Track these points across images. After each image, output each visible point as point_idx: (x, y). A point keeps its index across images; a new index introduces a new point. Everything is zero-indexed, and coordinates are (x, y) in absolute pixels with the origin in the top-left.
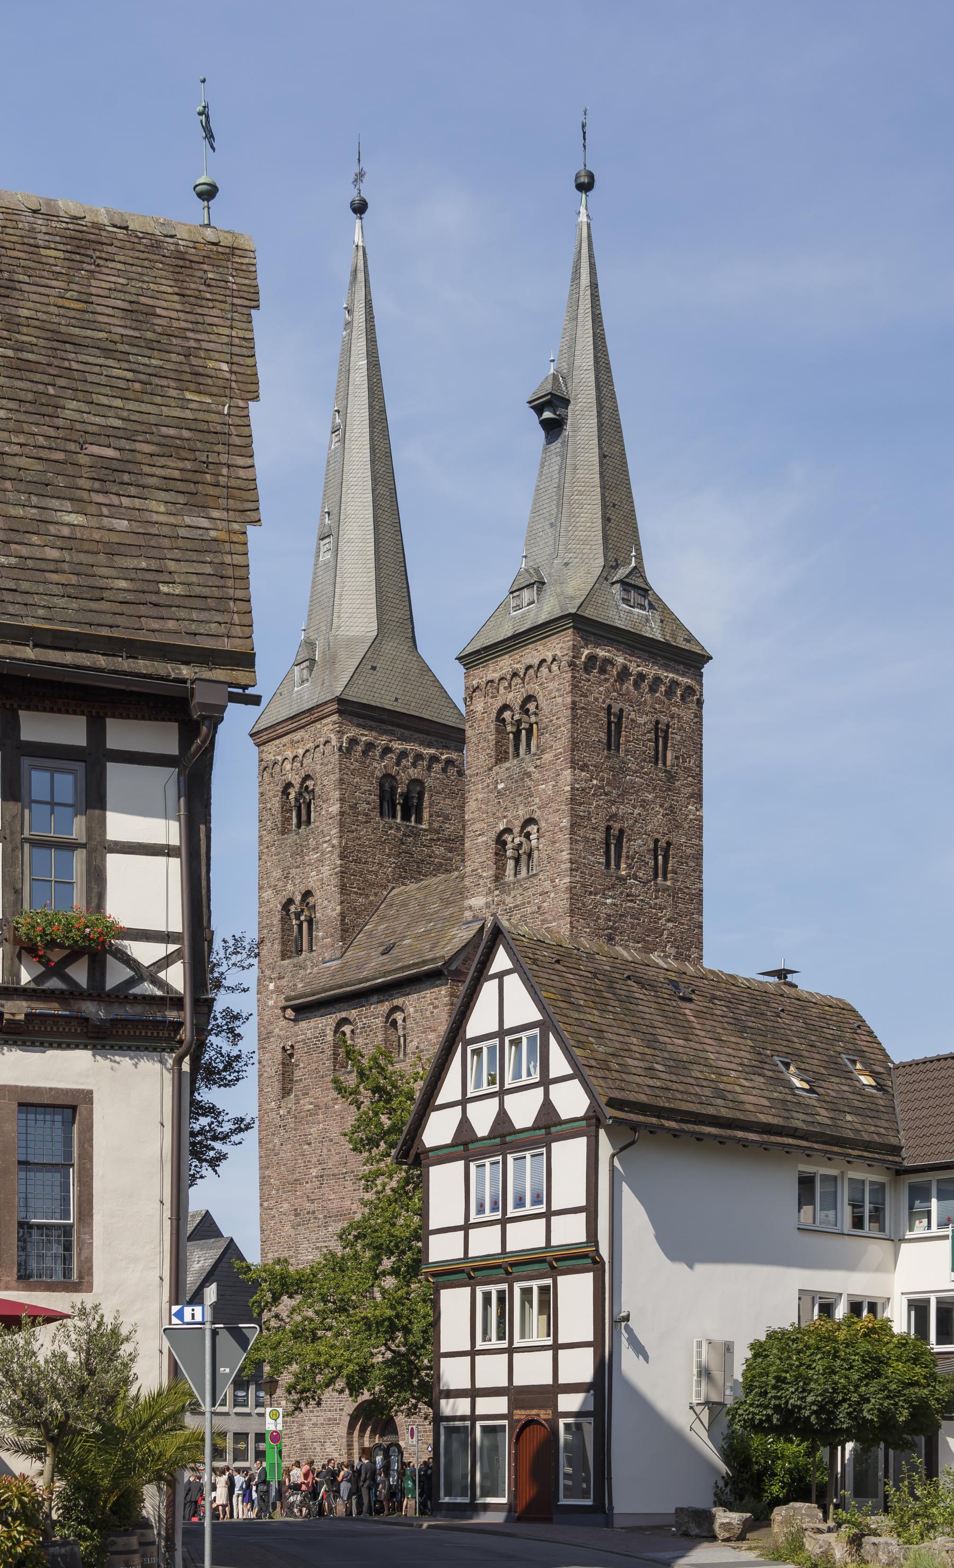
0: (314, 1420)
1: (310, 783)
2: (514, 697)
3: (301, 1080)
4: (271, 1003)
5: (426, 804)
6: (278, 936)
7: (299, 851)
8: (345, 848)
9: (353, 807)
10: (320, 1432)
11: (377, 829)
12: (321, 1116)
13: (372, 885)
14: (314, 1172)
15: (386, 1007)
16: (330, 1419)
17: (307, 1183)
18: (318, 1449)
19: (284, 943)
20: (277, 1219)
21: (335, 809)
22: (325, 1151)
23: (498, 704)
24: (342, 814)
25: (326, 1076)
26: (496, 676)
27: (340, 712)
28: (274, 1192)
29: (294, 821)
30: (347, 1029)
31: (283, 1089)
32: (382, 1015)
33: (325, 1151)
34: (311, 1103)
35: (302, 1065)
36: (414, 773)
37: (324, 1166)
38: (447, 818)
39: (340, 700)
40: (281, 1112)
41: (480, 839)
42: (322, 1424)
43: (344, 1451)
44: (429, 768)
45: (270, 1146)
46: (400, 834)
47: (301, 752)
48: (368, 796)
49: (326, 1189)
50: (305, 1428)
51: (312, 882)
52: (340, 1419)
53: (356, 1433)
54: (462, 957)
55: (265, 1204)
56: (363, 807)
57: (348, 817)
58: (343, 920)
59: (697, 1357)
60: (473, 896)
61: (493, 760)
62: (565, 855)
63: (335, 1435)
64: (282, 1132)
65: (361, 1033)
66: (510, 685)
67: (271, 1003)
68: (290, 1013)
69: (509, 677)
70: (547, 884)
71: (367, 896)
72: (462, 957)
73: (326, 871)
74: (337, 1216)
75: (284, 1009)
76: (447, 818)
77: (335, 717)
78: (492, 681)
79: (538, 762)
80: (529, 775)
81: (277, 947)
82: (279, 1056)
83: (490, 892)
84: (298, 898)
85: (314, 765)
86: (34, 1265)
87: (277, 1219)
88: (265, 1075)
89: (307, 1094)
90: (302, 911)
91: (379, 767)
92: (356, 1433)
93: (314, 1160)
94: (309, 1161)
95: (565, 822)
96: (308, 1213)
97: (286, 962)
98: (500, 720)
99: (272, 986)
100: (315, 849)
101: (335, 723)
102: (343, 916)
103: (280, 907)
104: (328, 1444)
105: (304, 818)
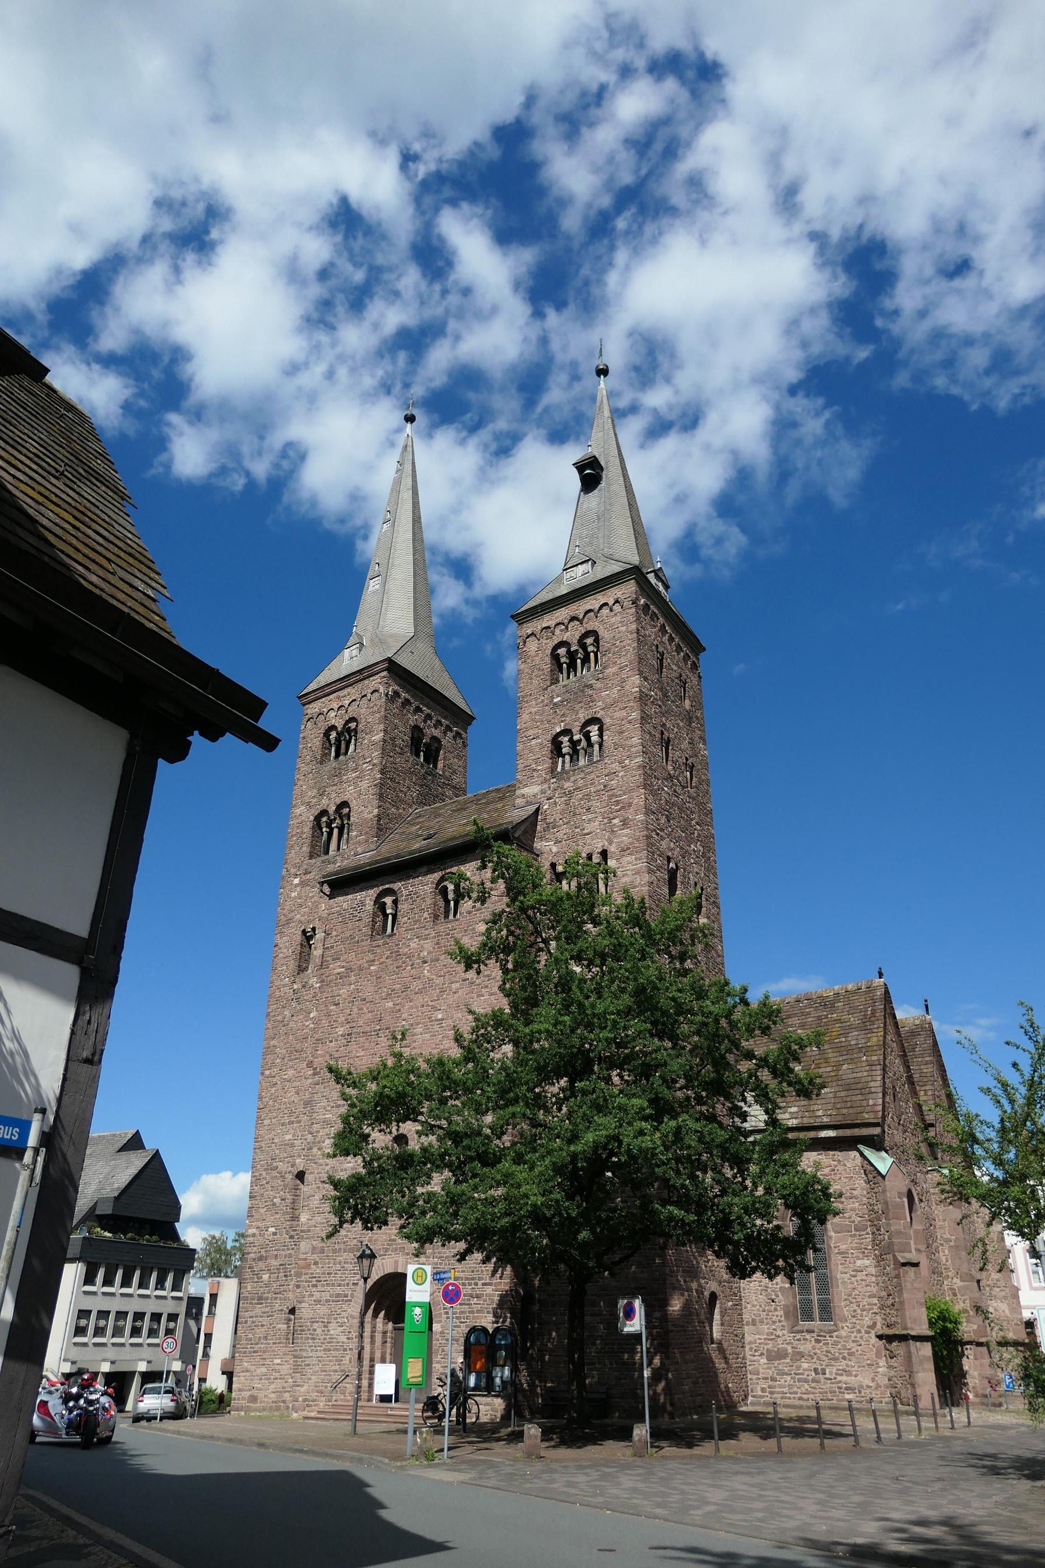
0: (317, 1295)
1: (353, 725)
2: (572, 635)
3: (332, 947)
4: (293, 894)
5: (441, 757)
6: (308, 841)
7: (337, 773)
8: (385, 767)
9: (393, 739)
10: (322, 1310)
11: (406, 761)
12: (353, 978)
13: (402, 801)
14: (340, 1031)
16: (338, 1295)
17: (331, 1042)
18: (319, 1331)
19: (313, 846)
20: (279, 1086)
21: (378, 737)
22: (355, 1010)
23: (551, 644)
24: (384, 741)
25: (362, 941)
26: (552, 623)
27: (387, 669)
28: (278, 1060)
29: (333, 754)
30: (388, 900)
31: (299, 966)
32: (432, 882)
33: (355, 1010)
35: (334, 933)
36: (436, 733)
37: (351, 1025)
38: (454, 772)
39: (389, 660)
40: (295, 987)
41: (534, 742)
42: (327, 1301)
43: (354, 1335)
44: (445, 733)
45: (279, 1018)
46: (423, 771)
47: (347, 702)
48: (404, 738)
49: (353, 1046)
50: (303, 1305)
51: (349, 793)
52: (352, 1296)
53: (370, 1312)
54: (523, 828)
55: (267, 1072)
56: (399, 742)
57: (388, 744)
58: (378, 823)
59: (810, 1301)
60: (526, 786)
61: (549, 683)
62: (636, 740)
63: (344, 1314)
64: (294, 1004)
65: (407, 900)
66: (567, 628)
67: (293, 894)
68: (327, 889)
69: (566, 621)
70: (616, 766)
71: (398, 808)
72: (523, 828)
73: (364, 784)
75: (322, 884)
76: (454, 772)
77: (385, 673)
78: (549, 627)
79: (601, 676)
80: (591, 686)
81: (306, 849)
82: (298, 937)
83: (546, 781)
84: (332, 809)
85: (362, 711)
86: (72, 1380)
87: (279, 1086)
88: (281, 955)
89: (338, 959)
90: (335, 819)
91: (414, 719)
92: (370, 1312)
93: (342, 1019)
95: (635, 715)
97: (313, 861)
98: (555, 657)
99: (296, 881)
100: (355, 770)
101: (384, 677)
102: (379, 817)
103: (312, 818)
104: (333, 1326)
105: (343, 750)
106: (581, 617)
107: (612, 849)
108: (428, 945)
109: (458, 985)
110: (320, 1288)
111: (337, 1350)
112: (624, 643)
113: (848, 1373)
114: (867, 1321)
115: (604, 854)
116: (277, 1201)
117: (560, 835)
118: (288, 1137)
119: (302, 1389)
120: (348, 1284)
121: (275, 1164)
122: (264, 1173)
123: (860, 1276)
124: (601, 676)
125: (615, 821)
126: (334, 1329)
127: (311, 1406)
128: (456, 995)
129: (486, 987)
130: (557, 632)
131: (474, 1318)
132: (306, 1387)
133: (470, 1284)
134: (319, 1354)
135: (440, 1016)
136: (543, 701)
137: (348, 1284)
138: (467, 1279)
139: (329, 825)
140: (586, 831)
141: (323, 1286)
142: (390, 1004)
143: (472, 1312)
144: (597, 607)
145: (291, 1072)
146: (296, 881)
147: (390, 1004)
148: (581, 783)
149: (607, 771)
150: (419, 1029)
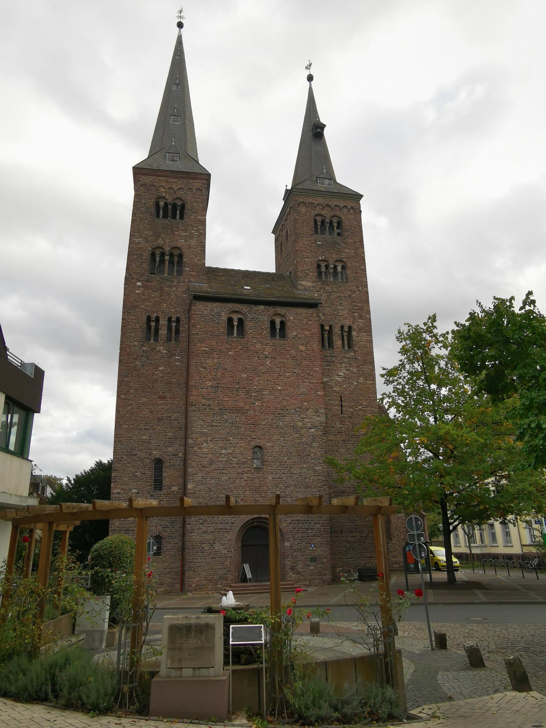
0: (204, 529)
4: (137, 291)
12: (216, 355)
14: (209, 384)
15: (272, 310)
23: (314, 213)
33: (220, 374)
34: (208, 347)
42: (212, 532)
60: (303, 280)
66: (324, 208)
74: (233, 410)
79: (344, 241)
83: (314, 282)
88: (128, 326)
94: (204, 377)
96: (205, 405)
106: (333, 207)
107: (355, 327)
108: (268, 348)
109: (290, 374)
110: (206, 525)
111: (221, 558)
112: (356, 230)
113: (395, 557)
114: (402, 537)
115: (350, 328)
116: (138, 474)
117: (326, 312)
118: (144, 437)
119: (195, 580)
120: (227, 523)
121: (134, 452)
122: (125, 457)
123: (400, 520)
124: (344, 241)
125: (356, 314)
126: (217, 546)
127: (202, 588)
128: (289, 380)
129: (308, 379)
130: (318, 208)
131: (310, 539)
132: (198, 578)
133: (306, 523)
134: (207, 560)
135: (279, 388)
136: (310, 240)
137: (227, 523)
138: (305, 520)
139: (163, 255)
140: (340, 314)
141: (208, 524)
142: (245, 376)
143: (309, 536)
144: (342, 206)
145: (144, 400)
146: (139, 284)
147: (245, 376)
148: (335, 290)
149: (350, 289)
150: (266, 392)
